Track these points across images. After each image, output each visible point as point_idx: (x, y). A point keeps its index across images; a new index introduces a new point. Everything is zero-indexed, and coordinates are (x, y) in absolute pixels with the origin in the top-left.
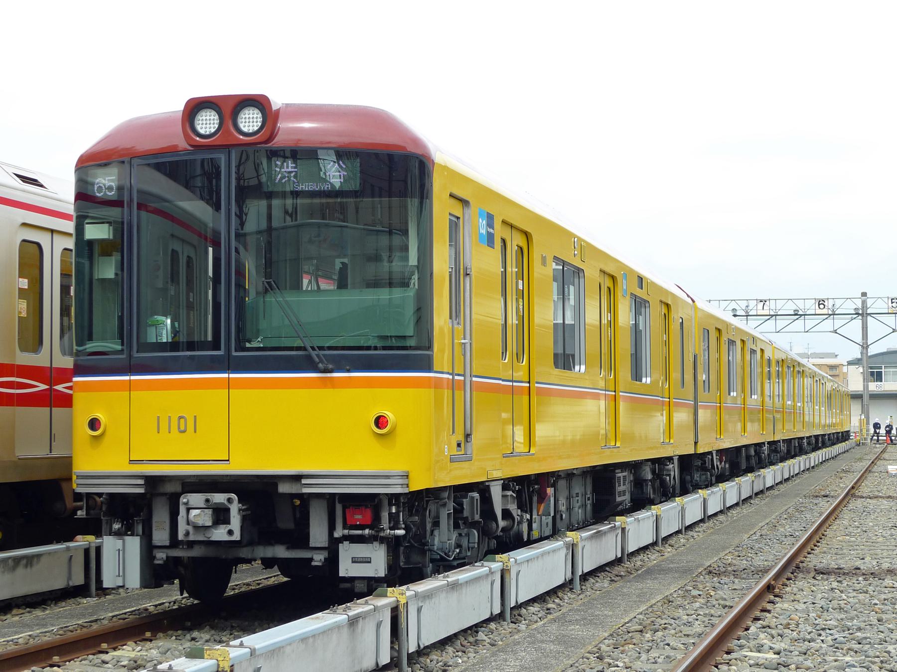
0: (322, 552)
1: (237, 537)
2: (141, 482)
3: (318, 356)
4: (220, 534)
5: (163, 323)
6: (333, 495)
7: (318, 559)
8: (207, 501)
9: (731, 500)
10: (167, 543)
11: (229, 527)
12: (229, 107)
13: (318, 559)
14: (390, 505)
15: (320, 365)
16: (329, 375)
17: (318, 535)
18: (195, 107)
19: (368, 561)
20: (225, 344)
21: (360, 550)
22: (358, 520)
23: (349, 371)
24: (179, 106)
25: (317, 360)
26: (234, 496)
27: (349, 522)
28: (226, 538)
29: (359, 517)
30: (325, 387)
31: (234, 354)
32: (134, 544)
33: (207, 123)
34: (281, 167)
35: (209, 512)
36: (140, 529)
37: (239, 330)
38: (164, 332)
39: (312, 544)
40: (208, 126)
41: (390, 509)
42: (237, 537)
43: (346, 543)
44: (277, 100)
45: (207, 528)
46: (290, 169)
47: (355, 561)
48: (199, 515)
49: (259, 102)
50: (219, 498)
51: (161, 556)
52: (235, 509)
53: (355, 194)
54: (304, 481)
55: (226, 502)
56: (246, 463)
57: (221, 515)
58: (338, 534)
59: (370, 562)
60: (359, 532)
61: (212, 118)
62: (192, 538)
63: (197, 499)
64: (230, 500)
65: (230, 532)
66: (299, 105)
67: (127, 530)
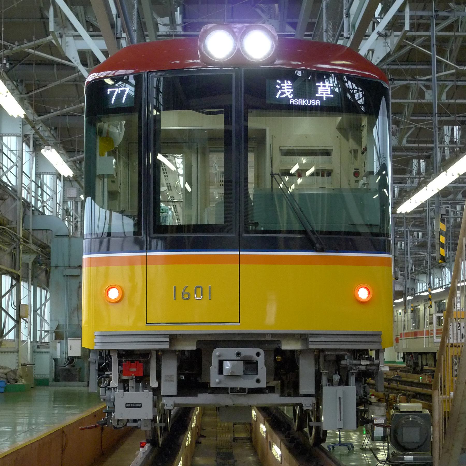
1: (263, 385)
3: (317, 238)
8: (238, 354)
11: (257, 377)
17: (307, 385)
19: (139, 406)
25: (315, 241)
29: (134, 370)
35: (242, 363)
47: (139, 406)
52: (261, 361)
54: (310, 339)
57: (250, 366)
59: (141, 407)
63: (231, 352)
64: (258, 354)
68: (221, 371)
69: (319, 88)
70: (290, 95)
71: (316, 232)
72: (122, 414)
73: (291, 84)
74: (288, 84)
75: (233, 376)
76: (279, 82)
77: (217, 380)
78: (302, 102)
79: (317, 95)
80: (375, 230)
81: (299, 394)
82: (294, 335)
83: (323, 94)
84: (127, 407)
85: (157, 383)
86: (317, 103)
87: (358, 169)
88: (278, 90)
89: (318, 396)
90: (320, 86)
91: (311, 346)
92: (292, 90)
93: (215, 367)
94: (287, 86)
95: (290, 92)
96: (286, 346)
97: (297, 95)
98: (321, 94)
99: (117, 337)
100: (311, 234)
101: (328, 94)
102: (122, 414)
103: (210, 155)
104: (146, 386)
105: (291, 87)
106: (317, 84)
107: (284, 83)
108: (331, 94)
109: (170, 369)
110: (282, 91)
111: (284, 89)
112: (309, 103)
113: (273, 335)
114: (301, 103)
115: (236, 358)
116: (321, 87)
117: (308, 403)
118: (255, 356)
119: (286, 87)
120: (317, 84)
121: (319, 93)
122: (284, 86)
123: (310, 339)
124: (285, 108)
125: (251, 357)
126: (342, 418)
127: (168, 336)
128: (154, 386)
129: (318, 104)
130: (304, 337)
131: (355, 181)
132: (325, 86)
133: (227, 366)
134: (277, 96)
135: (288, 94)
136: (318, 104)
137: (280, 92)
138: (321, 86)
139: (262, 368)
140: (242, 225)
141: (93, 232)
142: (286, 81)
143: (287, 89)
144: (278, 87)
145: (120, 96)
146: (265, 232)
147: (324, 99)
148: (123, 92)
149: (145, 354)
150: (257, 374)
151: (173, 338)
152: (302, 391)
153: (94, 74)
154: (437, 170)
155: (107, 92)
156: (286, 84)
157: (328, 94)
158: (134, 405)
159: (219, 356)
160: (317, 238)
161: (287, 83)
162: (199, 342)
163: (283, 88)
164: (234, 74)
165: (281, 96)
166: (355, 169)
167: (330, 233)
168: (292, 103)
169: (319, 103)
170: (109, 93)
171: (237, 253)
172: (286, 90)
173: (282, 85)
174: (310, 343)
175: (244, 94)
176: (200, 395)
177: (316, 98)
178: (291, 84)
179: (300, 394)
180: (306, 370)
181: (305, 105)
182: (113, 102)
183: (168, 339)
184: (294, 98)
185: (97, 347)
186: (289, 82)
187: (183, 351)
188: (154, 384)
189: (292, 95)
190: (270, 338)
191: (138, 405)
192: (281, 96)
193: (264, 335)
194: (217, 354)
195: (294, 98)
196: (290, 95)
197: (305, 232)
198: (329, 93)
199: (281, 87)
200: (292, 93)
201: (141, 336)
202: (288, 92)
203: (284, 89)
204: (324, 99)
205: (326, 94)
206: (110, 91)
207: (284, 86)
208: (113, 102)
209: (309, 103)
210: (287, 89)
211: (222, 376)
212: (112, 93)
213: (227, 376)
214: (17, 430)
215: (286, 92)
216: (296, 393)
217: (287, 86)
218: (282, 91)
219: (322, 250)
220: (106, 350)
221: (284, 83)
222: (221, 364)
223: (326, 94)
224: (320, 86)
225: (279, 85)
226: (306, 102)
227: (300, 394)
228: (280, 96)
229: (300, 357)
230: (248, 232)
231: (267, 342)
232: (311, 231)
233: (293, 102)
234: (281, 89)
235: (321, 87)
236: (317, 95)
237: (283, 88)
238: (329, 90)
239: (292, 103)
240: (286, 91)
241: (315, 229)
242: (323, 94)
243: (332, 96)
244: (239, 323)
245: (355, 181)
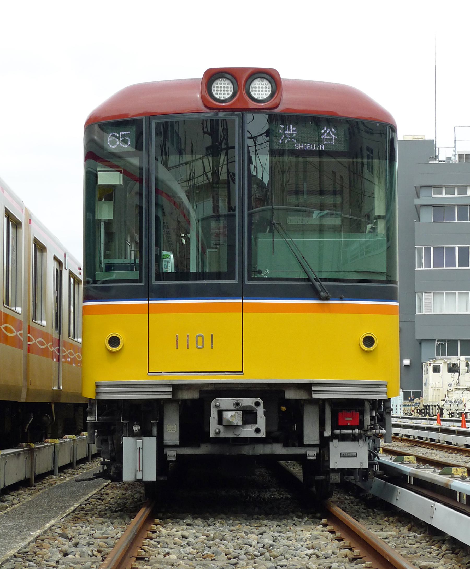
0: (314, 448)
1: (263, 434)
2: (170, 389)
3: (321, 286)
4: (248, 432)
5: (168, 257)
6: (324, 400)
7: (312, 454)
8: (237, 404)
9: (64, 459)
10: (177, 443)
11: (256, 426)
12: (242, 78)
13: (312, 454)
14: (371, 410)
15: (322, 294)
16: (326, 302)
17: (311, 434)
18: (213, 75)
19: (354, 455)
20: (230, 275)
21: (348, 447)
22: (349, 421)
23: (341, 299)
24: (199, 74)
25: (320, 289)
26: (260, 400)
27: (340, 423)
28: (254, 435)
29: (350, 419)
30: (323, 312)
31: (247, 283)
32: (150, 443)
33: (223, 90)
34: (284, 129)
35: (240, 413)
36: (155, 430)
37: (250, 264)
38: (169, 265)
39: (306, 442)
40: (222, 92)
41: (371, 413)
42: (263, 434)
43: (336, 441)
44: (284, 75)
45: (237, 426)
46: (291, 132)
47: (343, 455)
48: (234, 415)
49: (270, 75)
50: (248, 402)
51: (171, 454)
52: (261, 411)
53: (114, 203)
54: (314, 389)
55: (254, 405)
56: (256, 374)
57: (249, 416)
58: (327, 433)
59: (356, 457)
60: (350, 432)
61: (226, 86)
62: (222, 435)
63: (225, 403)
64: (257, 404)
65: (258, 431)
66: (293, 80)
67: (145, 432)
71: (319, 280)
76: (282, 126)
81: (303, 442)
84: (341, 457)
91: (315, 396)
96: (290, 395)
123: (314, 389)
126: (141, 469)
130: (307, 387)
133: (228, 415)
151: (176, 388)
160: (321, 286)
162: (201, 392)
164: (144, 118)
171: (240, 301)
179: (305, 443)
183: (170, 389)
187: (185, 401)
191: (353, 455)
197: (308, 280)
201: (160, 386)
214: (339, 481)
216: (301, 444)
222: (220, 413)
227: (305, 443)
230: (250, 279)
233: (298, 147)
244: (242, 372)
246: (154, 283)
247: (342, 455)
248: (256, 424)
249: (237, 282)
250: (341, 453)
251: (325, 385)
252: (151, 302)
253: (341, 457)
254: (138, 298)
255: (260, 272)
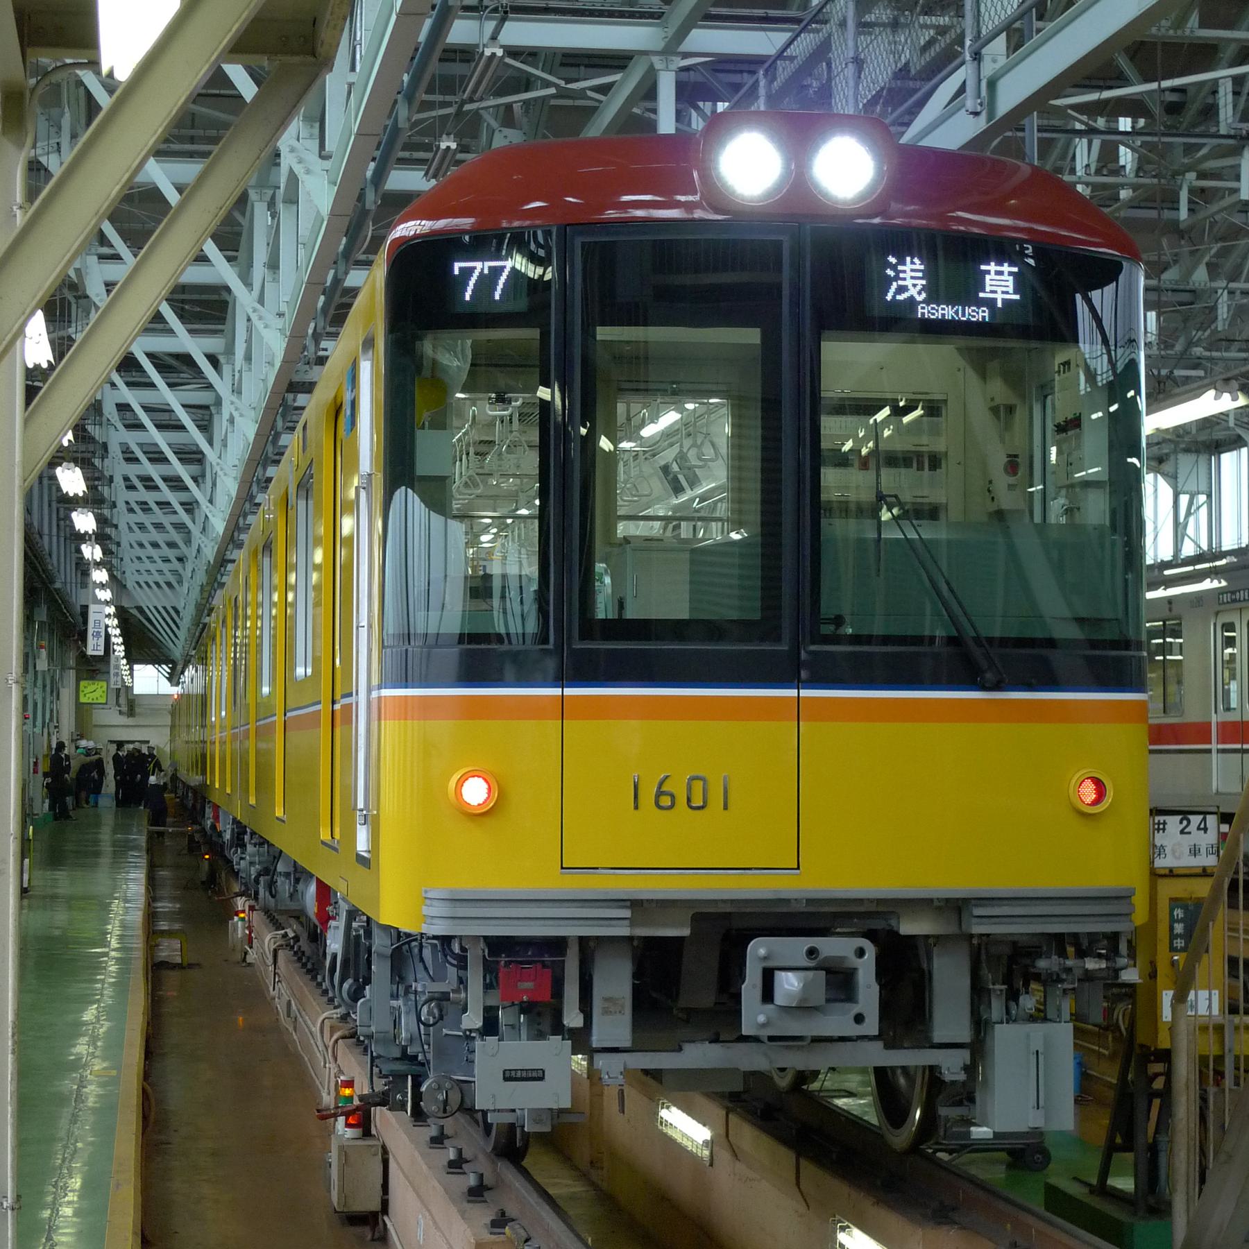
11: (856, 1009)
17: (950, 1018)
19: (509, 1076)
22: (526, 991)
25: (984, 664)
29: (529, 985)
50: (836, 947)
57: (840, 982)
59: (541, 1079)
68: (768, 994)
69: (988, 277)
70: (919, 293)
72: (494, 1096)
73: (922, 267)
74: (914, 267)
75: (803, 1009)
76: (892, 260)
77: (761, 1019)
78: (947, 312)
79: (981, 295)
80: (1108, 634)
82: (929, 901)
83: (995, 292)
84: (506, 1079)
85: (581, 1016)
86: (982, 314)
87: (1016, 456)
88: (889, 281)
89: (978, 1047)
90: (988, 272)
92: (924, 282)
93: (754, 986)
94: (912, 270)
95: (919, 287)
96: (908, 927)
97: (934, 296)
98: (992, 292)
99: (492, 904)
100: (971, 643)
101: (1007, 293)
102: (494, 1096)
103: (621, 408)
104: (558, 1028)
105: (920, 274)
106: (983, 267)
107: (904, 264)
108: (1015, 293)
109: (615, 983)
110: (900, 283)
111: (904, 279)
112: (964, 315)
113: (879, 901)
114: (943, 315)
115: (805, 962)
116: (993, 276)
117: (952, 1065)
118: (851, 955)
119: (909, 274)
120: (983, 267)
121: (988, 289)
122: (904, 272)
124: (898, 322)
125: (843, 958)
127: (628, 904)
128: (572, 1025)
129: (984, 317)
130: (957, 907)
131: (1009, 485)
132: (1001, 273)
134: (889, 297)
135: (913, 292)
136: (984, 317)
137: (894, 286)
138: (993, 273)
139: (869, 987)
140: (787, 617)
141: (412, 631)
142: (908, 259)
143: (912, 278)
144: (890, 272)
145: (488, 281)
146: (856, 639)
147: (999, 305)
148: (496, 272)
149: (557, 945)
150: (856, 1002)
152: (939, 1035)
153: (412, 223)
154: (796, 303)
155: (453, 270)
156: (908, 267)
157: (1007, 293)
158: (524, 1075)
159: (765, 958)
161: (912, 263)
163: (902, 275)
165: (898, 297)
166: (1009, 456)
167: (1021, 642)
168: (923, 314)
169: (986, 314)
170: (456, 272)
172: (909, 279)
173: (900, 268)
174: (974, 920)
175: (800, 287)
176: (688, 1047)
177: (981, 303)
178: (922, 267)
180: (949, 979)
181: (953, 320)
182: (468, 298)
184: (927, 302)
185: (440, 929)
186: (916, 260)
188: (573, 1019)
189: (924, 295)
190: (873, 908)
191: (535, 1074)
192: (898, 297)
193: (860, 901)
194: (762, 952)
195: (927, 302)
196: (919, 293)
198: (1011, 290)
199: (898, 272)
200: (924, 288)
201: (551, 904)
202: (914, 286)
203: (904, 279)
204: (999, 305)
205: (1003, 292)
206: (461, 269)
207: (904, 272)
208: (468, 298)
209: (964, 315)
210: (912, 278)
211: (771, 1006)
212: (467, 273)
213: (786, 1009)
215: (910, 287)
217: (912, 270)
218: (900, 283)
219: (997, 687)
220: (924, 1067)
221: (904, 264)
222: (768, 976)
223: (1003, 292)
224: (988, 272)
225: (894, 267)
226: (957, 313)
228: (894, 297)
229: (935, 951)
231: (871, 918)
232: (973, 638)
233: (924, 311)
234: (897, 278)
235: (993, 276)
236: (981, 295)
237: (902, 275)
238: (1011, 283)
239: (923, 314)
240: (909, 283)
241: (984, 633)
242: (995, 292)
243: (1017, 297)
245: (1009, 485)
246: (551, 646)
247: (507, 1075)
248: (856, 1002)
249: (786, 648)
250: (504, 1071)
251: (995, 902)
252: (568, 691)
253: (506, 1079)
254: (485, 680)
255: (838, 621)
